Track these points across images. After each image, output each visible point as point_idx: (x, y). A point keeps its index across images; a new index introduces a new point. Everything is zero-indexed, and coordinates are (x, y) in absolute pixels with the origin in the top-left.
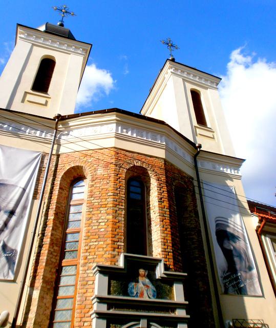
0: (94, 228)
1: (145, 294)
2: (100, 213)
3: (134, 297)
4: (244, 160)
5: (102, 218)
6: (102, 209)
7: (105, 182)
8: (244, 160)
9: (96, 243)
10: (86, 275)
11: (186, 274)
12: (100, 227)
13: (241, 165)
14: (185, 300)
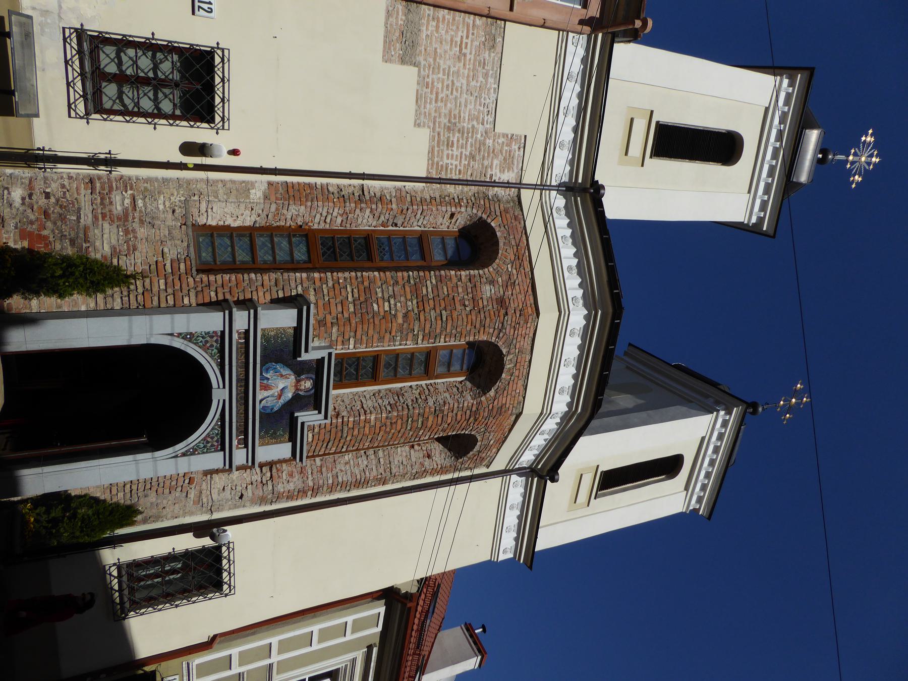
0: (379, 290)
1: (266, 393)
3: (261, 374)
5: (399, 304)
6: (415, 302)
7: (467, 303)
9: (350, 299)
11: (799, 75)
12: (380, 302)
14: (752, 223)
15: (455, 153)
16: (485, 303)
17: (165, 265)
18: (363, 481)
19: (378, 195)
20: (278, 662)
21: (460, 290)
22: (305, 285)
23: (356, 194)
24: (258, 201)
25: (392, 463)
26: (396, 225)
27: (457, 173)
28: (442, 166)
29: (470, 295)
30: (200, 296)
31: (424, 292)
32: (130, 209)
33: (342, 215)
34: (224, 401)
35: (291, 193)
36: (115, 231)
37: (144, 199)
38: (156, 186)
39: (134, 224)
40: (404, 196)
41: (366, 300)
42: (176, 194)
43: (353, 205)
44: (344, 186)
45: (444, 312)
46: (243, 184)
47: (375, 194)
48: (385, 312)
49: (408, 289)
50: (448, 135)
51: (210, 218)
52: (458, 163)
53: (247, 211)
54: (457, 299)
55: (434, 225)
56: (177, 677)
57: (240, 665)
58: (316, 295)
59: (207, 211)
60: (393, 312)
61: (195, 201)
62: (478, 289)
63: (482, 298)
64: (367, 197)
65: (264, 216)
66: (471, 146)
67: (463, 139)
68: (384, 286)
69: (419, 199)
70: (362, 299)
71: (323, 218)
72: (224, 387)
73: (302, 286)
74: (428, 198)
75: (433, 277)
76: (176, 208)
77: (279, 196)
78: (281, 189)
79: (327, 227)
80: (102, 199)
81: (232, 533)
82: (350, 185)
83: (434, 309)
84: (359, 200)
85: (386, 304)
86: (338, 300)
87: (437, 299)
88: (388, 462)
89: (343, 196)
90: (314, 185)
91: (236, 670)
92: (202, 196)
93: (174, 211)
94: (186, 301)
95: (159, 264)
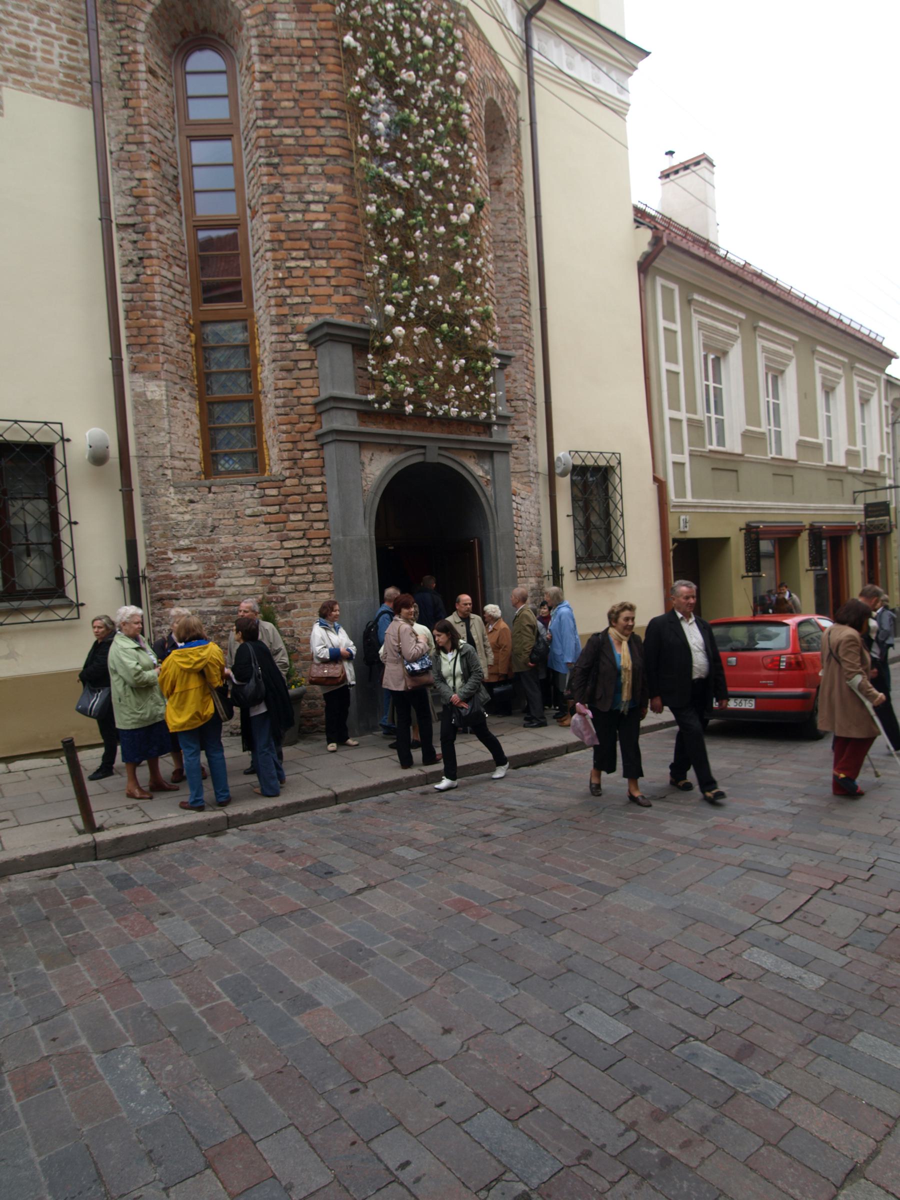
0: (292, 217)
2: (305, 173)
4: (647, 54)
5: (315, 188)
6: (309, 160)
7: (308, 69)
8: (647, 54)
9: (307, 264)
10: (289, 346)
11: (119, 748)
12: (309, 217)
13: (631, 75)
15: (39, 45)
16: (307, 34)
17: (270, 514)
18: (521, 283)
19: (131, 201)
20: (687, 412)
21: (286, 77)
22: (289, 330)
23: (135, 237)
24: (164, 388)
25: (504, 238)
26: (176, 177)
27: (74, 47)
28: (67, 76)
29: (295, 60)
30: (311, 471)
31: (291, 141)
32: (193, 554)
33: (170, 266)
34: (440, 448)
35: (144, 340)
36: (227, 571)
37: (178, 538)
38: (157, 523)
39: (215, 550)
40: (128, 154)
41: (309, 239)
42: (166, 499)
43: (154, 245)
44: (123, 256)
45: (325, 112)
46: (140, 408)
47: (131, 206)
48: (325, 211)
49: (288, 169)
50: (7, 51)
51: (192, 456)
52: (56, 43)
53: (178, 405)
54: (302, 86)
55: (170, 110)
56: (682, 517)
57: (682, 453)
58: (304, 315)
59: (185, 460)
60: (326, 198)
61: (173, 474)
62: (283, 43)
63: (299, 40)
64: (138, 219)
65: (182, 384)
66: (21, 8)
67: (11, 24)
68: (287, 209)
69: (131, 130)
70: (306, 245)
71: (178, 295)
72: (424, 447)
73: (291, 334)
74: (126, 112)
75: (267, 122)
76: (187, 498)
77: (152, 358)
78: (141, 355)
79: (187, 290)
80: (184, 587)
81: (560, 452)
82: (121, 246)
83: (318, 128)
84: (143, 233)
85: (313, 207)
86: (309, 282)
87: (302, 122)
88: (501, 245)
89: (141, 259)
90: (128, 304)
91: (685, 458)
92: (166, 465)
93: (191, 502)
94: (318, 488)
95: (269, 520)
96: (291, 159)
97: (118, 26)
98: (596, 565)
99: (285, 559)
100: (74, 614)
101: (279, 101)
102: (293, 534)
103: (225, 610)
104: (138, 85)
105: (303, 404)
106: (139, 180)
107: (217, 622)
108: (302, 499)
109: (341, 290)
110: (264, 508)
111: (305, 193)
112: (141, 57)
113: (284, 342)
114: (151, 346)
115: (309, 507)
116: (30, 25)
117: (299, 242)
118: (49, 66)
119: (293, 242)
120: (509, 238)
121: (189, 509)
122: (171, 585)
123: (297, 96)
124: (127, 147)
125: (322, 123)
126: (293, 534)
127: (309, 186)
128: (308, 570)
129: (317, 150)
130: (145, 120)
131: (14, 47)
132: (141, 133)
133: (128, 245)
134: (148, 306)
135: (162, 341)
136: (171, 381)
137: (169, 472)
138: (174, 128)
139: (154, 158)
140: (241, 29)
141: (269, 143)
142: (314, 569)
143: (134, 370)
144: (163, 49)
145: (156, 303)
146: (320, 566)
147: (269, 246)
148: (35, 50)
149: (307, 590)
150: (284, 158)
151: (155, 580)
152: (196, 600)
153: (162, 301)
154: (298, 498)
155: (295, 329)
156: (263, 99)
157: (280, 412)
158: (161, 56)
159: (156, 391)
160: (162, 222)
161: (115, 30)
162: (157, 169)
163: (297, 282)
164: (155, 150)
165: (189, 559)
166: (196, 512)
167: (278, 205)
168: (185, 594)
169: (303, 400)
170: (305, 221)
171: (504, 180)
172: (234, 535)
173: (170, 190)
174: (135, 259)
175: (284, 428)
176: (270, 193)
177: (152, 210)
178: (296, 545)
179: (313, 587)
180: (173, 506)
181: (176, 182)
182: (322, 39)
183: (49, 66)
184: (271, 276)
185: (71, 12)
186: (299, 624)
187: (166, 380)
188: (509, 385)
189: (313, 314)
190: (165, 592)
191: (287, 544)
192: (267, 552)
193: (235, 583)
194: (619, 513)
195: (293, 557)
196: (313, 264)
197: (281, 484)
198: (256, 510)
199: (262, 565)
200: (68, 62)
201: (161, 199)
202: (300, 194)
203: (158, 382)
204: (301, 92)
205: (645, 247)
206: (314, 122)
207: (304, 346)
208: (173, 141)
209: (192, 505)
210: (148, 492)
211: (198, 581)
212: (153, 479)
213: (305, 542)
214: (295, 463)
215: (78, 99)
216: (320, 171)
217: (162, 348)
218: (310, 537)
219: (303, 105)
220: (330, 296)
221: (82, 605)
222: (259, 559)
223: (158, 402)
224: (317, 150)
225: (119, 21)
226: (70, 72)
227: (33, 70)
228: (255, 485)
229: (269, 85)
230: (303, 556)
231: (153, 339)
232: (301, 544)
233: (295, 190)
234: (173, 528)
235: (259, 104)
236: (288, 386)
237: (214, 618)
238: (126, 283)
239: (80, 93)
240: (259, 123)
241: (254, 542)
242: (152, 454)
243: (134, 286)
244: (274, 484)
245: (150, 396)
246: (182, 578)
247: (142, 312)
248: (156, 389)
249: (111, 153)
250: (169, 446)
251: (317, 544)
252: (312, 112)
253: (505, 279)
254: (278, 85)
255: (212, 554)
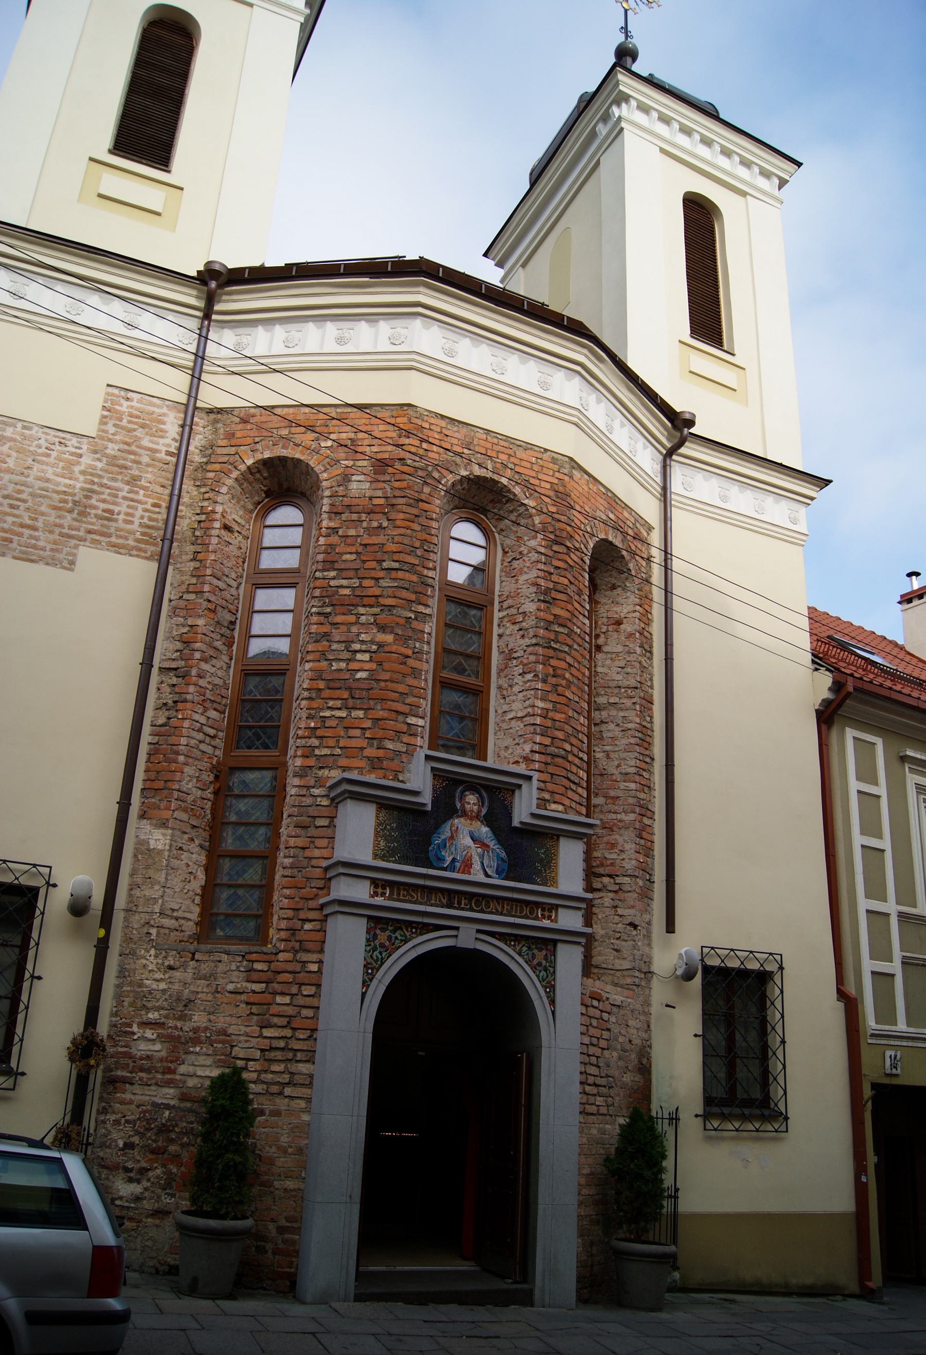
0: (335, 666)
2: (356, 623)
5: (363, 637)
6: (362, 610)
7: (375, 524)
9: (343, 714)
12: (353, 666)
17: (254, 992)
19: (179, 645)
21: (352, 532)
22: (312, 783)
23: (174, 680)
24: (169, 837)
25: (620, 684)
26: (233, 623)
27: (157, 510)
29: (364, 516)
30: (310, 946)
31: (347, 592)
33: (206, 709)
34: (478, 931)
35: (160, 784)
37: (148, 1010)
39: (186, 1028)
40: (186, 603)
41: (350, 689)
42: (144, 962)
43: (192, 689)
44: (159, 698)
45: (385, 565)
46: (140, 857)
47: (177, 651)
48: (371, 660)
49: (339, 619)
50: (93, 516)
52: (140, 507)
55: (240, 561)
56: (888, 1053)
58: (330, 768)
59: (177, 919)
60: (374, 647)
61: (158, 933)
62: (355, 502)
63: (371, 498)
65: (193, 833)
67: (103, 493)
69: (194, 581)
70: (346, 695)
71: (208, 740)
72: (457, 928)
73: (314, 787)
74: (193, 565)
75: (326, 573)
77: (162, 805)
80: (142, 1070)
83: (377, 579)
84: (183, 677)
85: (359, 656)
86: (342, 733)
87: (361, 573)
88: (617, 691)
89: (175, 702)
90: (152, 746)
91: (895, 967)
92: (152, 922)
94: (314, 967)
95: (252, 1000)
96: (343, 609)
97: (203, 490)
98: (737, 1111)
99: (262, 1050)
100: (9, 1083)
101: (342, 554)
102: (275, 1020)
103: (182, 1105)
104: (210, 540)
105: (313, 867)
106: (191, 626)
107: (169, 1119)
108: (294, 979)
109: (375, 743)
110: (249, 985)
111: (352, 642)
112: (218, 516)
113: (304, 796)
114: (165, 792)
115: (300, 990)
116: (120, 493)
117: (338, 691)
118: (128, 527)
119: (332, 691)
120: (626, 683)
121: (167, 976)
122: (128, 1065)
123: (360, 549)
124: (186, 596)
125: (381, 574)
126: (275, 1020)
127: (358, 635)
128: (286, 1067)
129: (372, 601)
130: (209, 572)
131: (100, 512)
132: (203, 583)
133: (166, 689)
134: (172, 750)
135: (177, 787)
136: (179, 830)
137: (154, 931)
138: (242, 577)
139: (212, 607)
140: (318, 489)
141: (324, 594)
142: (293, 1067)
143: (143, 816)
144: (244, 507)
145: (181, 747)
146: (301, 1065)
147: (306, 694)
148: (119, 514)
149: (281, 1093)
150: (337, 607)
151: (112, 1057)
152: (153, 1088)
153: (187, 745)
154: (288, 977)
155: (320, 782)
156: (326, 552)
157: (286, 874)
158: (241, 513)
159: (159, 839)
160: (204, 666)
161: (200, 493)
162: (212, 615)
163: (329, 733)
164: (213, 599)
165: (155, 1036)
166: (173, 981)
167: (323, 653)
168: (141, 1079)
169: (314, 862)
170: (349, 670)
171: (625, 621)
172: (210, 1013)
173: (222, 635)
174: (170, 702)
175: (287, 892)
176: (317, 641)
177: (197, 655)
178: (277, 1034)
179: (288, 1091)
180: (150, 971)
181: (232, 627)
182: (395, 497)
183: (128, 527)
184: (303, 725)
185: (161, 480)
186: (263, 1136)
187: (173, 829)
188: (615, 856)
189: (341, 767)
190: (120, 1073)
191: (267, 1032)
192: (242, 1038)
193: (199, 1073)
194: (779, 1039)
195: (272, 1049)
196: (349, 715)
197: (273, 957)
198: (239, 986)
199: (233, 1054)
200: (148, 522)
201: (210, 646)
202: (348, 642)
203: (163, 831)
204: (365, 545)
205: (826, 694)
206: (373, 574)
207: (325, 802)
208: (237, 588)
209: (172, 972)
210: (127, 952)
211: (159, 1065)
212: (135, 938)
213: (288, 1032)
214: (294, 934)
215: (149, 553)
216: (372, 620)
217: (176, 794)
218: (294, 1026)
219: (365, 558)
220: (362, 749)
221: (23, 1074)
222: (232, 1046)
223: (160, 852)
224: (372, 601)
225: (205, 485)
226: (147, 530)
227: (112, 530)
228: (243, 956)
229: (334, 539)
230: (282, 1049)
231: (169, 784)
232: (283, 1034)
233: (343, 639)
234: (144, 996)
235: (320, 557)
236: (300, 845)
237: (167, 1113)
238: (155, 726)
239: (152, 548)
240: (318, 574)
241: (230, 1025)
242: (140, 909)
243: (163, 729)
244: (266, 957)
245: (152, 844)
246: (141, 1059)
247: (164, 755)
248: (161, 837)
249: (170, 601)
250: (160, 901)
251: (302, 1037)
252: (373, 564)
253: (617, 729)
254: (343, 539)
255: (181, 1033)
